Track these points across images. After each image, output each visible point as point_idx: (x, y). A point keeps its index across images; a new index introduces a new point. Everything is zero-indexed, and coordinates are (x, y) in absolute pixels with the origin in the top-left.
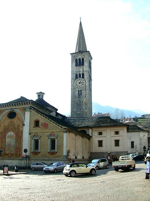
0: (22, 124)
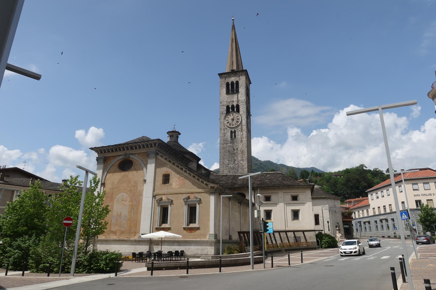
0: (142, 180)
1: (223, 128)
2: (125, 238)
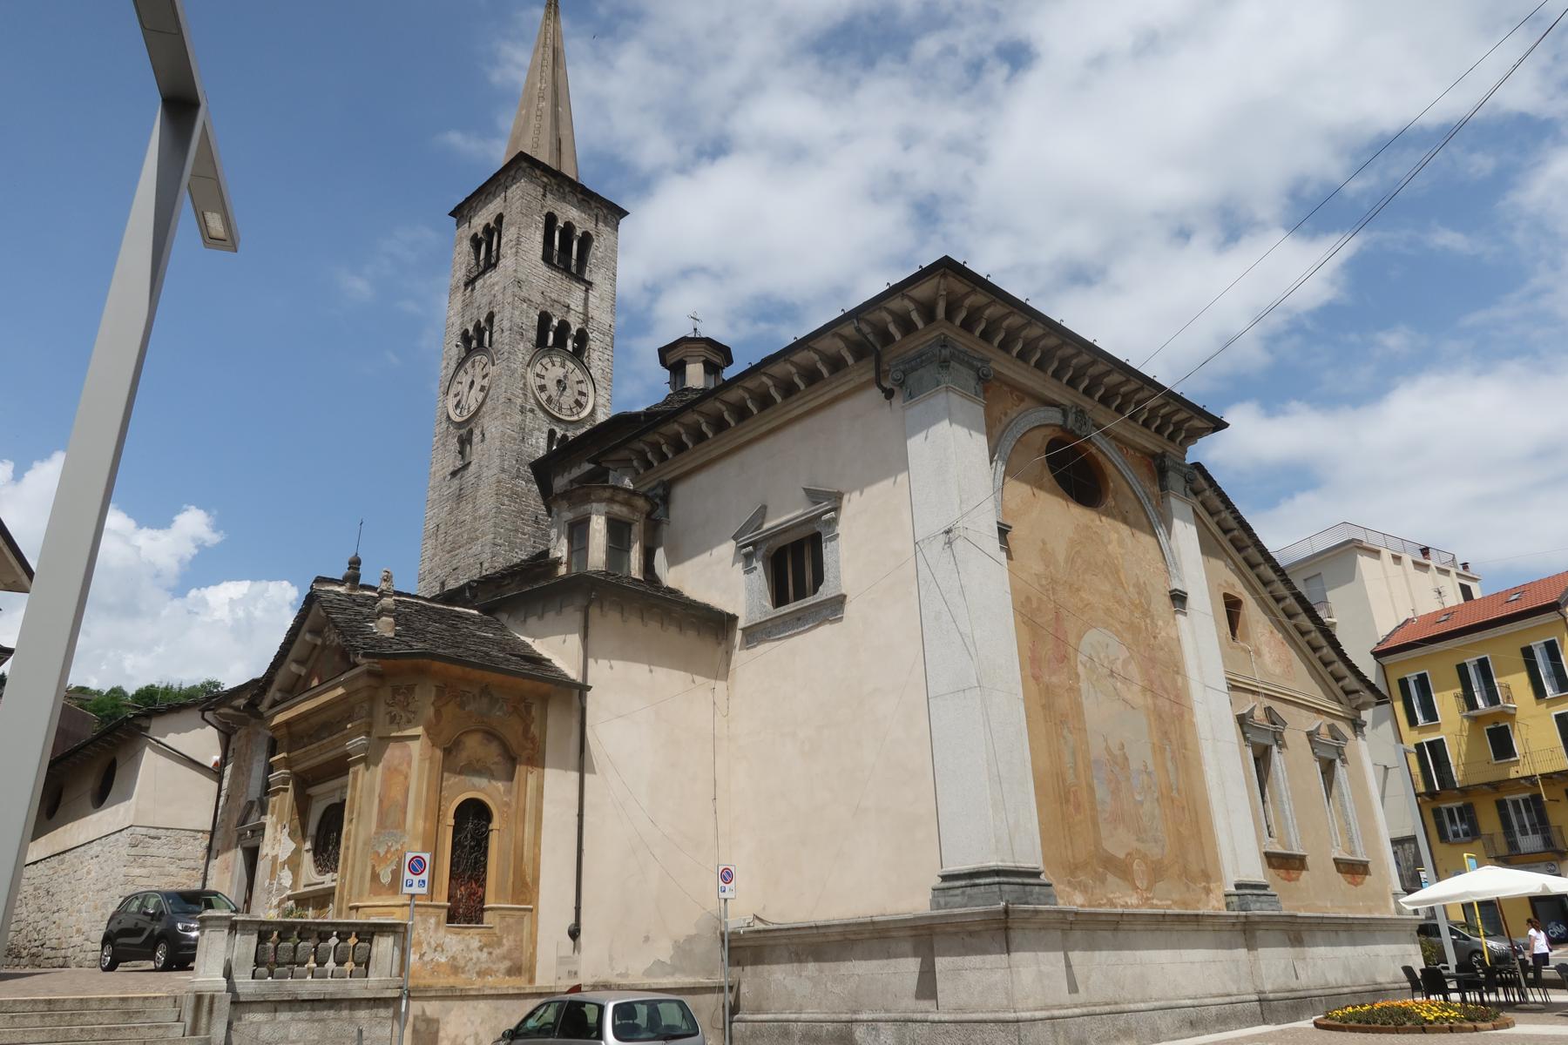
1: (519, 401)
2: (1175, 902)
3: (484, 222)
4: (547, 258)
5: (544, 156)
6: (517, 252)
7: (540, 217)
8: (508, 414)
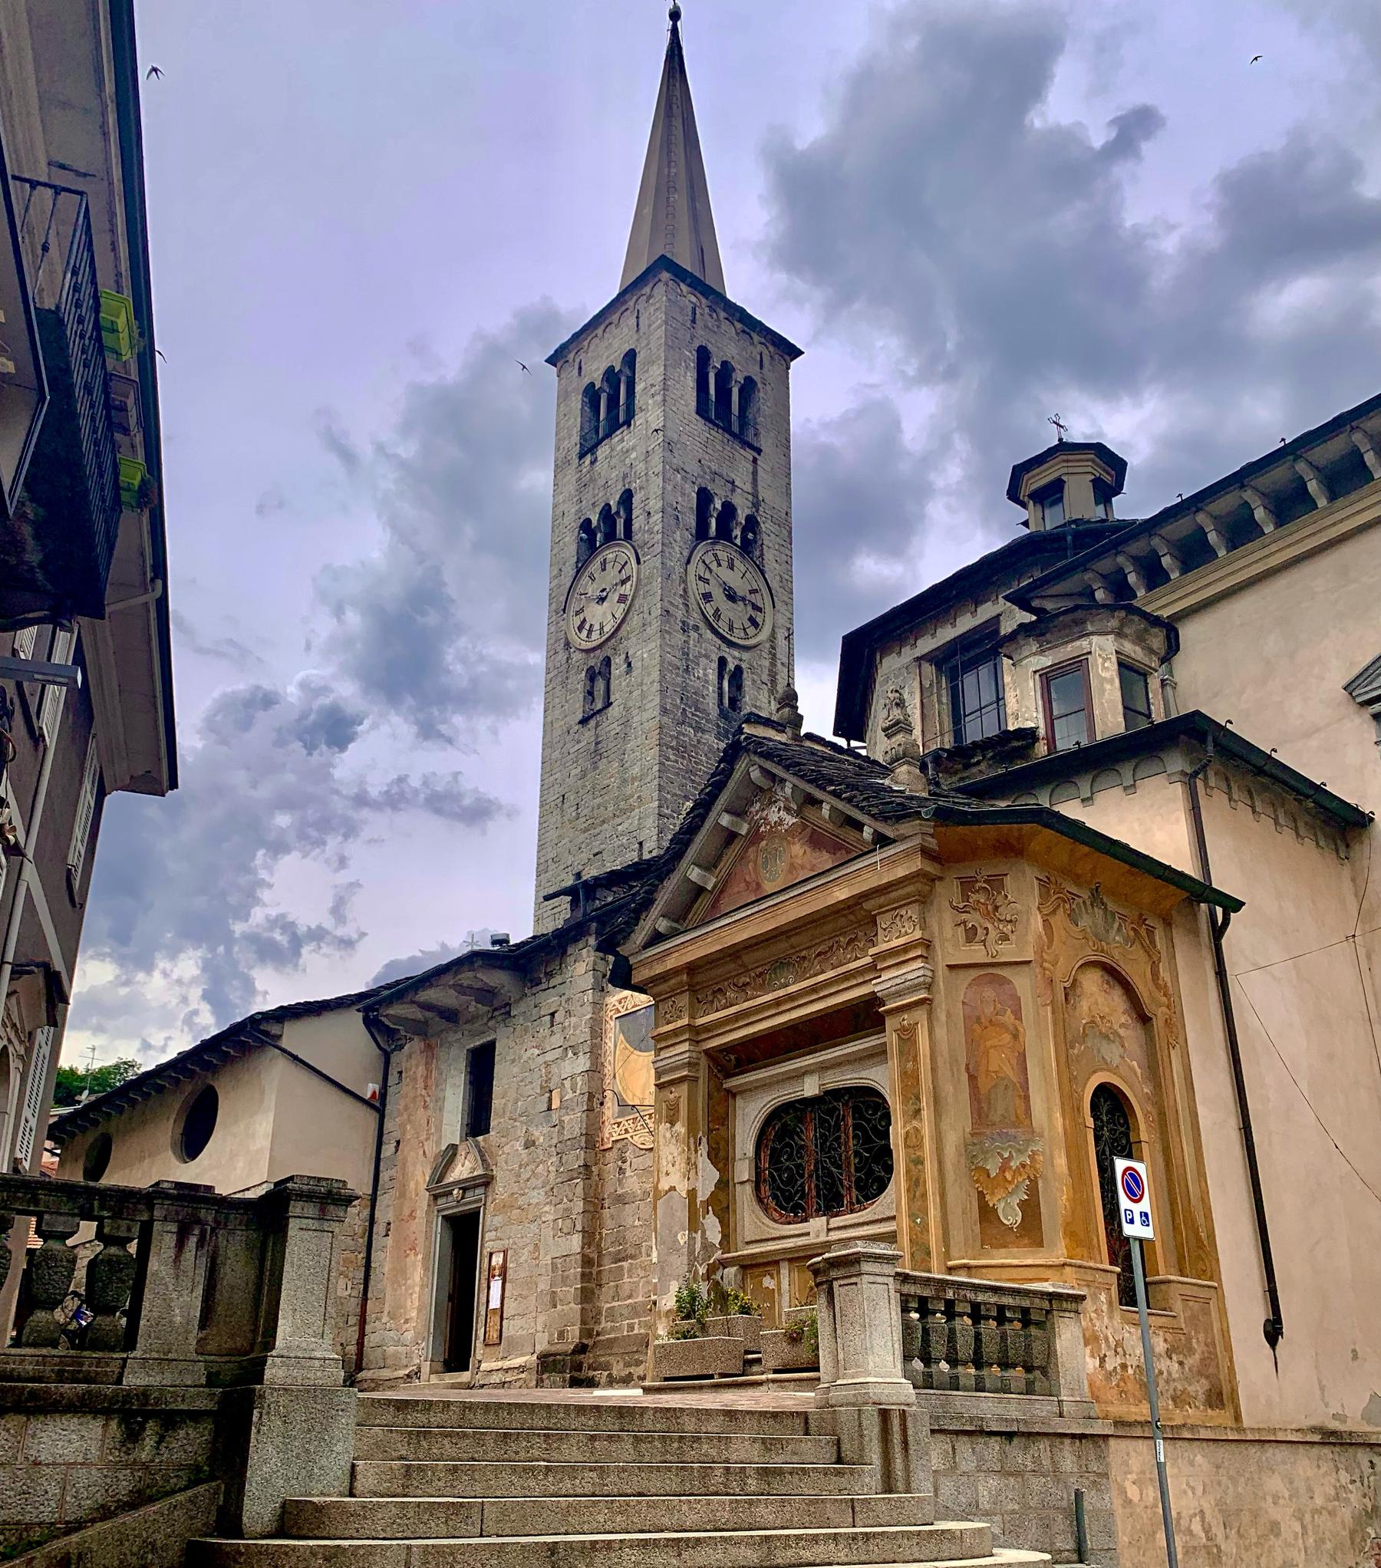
3: (603, 366)
4: (702, 410)
5: (686, 262)
6: (664, 400)
7: (690, 352)
8: (667, 632)
